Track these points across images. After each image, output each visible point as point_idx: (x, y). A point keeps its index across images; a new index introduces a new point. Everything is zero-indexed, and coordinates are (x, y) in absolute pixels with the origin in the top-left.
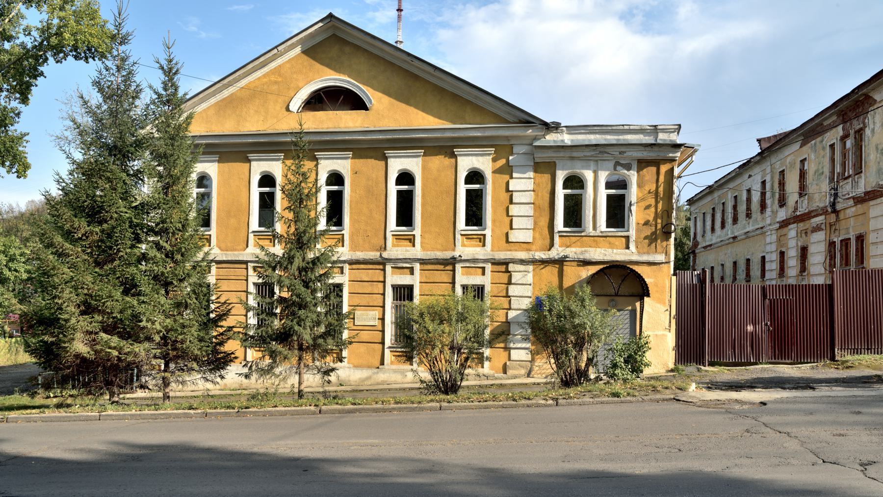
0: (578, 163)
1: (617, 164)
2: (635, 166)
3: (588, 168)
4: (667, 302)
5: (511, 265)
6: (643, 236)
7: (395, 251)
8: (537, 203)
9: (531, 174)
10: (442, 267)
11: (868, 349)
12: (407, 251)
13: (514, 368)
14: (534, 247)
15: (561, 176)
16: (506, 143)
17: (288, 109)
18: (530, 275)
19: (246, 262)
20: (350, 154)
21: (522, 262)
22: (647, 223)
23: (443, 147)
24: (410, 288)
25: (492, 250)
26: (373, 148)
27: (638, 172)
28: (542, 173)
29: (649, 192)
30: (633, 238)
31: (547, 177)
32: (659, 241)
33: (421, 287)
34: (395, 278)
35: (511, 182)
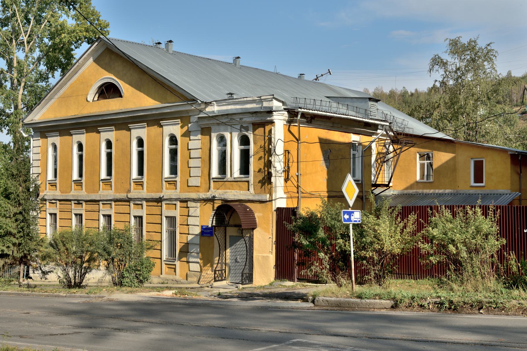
0: (222, 127)
1: (242, 127)
2: (251, 127)
3: (226, 130)
4: (271, 231)
5: (189, 202)
6: (258, 181)
7: (167, 192)
8: (202, 157)
9: (199, 137)
10: (155, 204)
11: (409, 275)
12: (140, 193)
13: (191, 277)
14: (201, 189)
15: (214, 136)
16: (187, 115)
17: (87, 101)
18: (198, 210)
19: (70, 200)
20: (113, 128)
21: (194, 200)
22: (260, 171)
23: (154, 119)
24: (174, 218)
25: (180, 192)
26: (123, 122)
27: (253, 132)
28: (205, 135)
29: (261, 147)
30: (252, 182)
31: (208, 137)
32: (266, 184)
33: (180, 218)
34: (167, 211)
35: (190, 142)
